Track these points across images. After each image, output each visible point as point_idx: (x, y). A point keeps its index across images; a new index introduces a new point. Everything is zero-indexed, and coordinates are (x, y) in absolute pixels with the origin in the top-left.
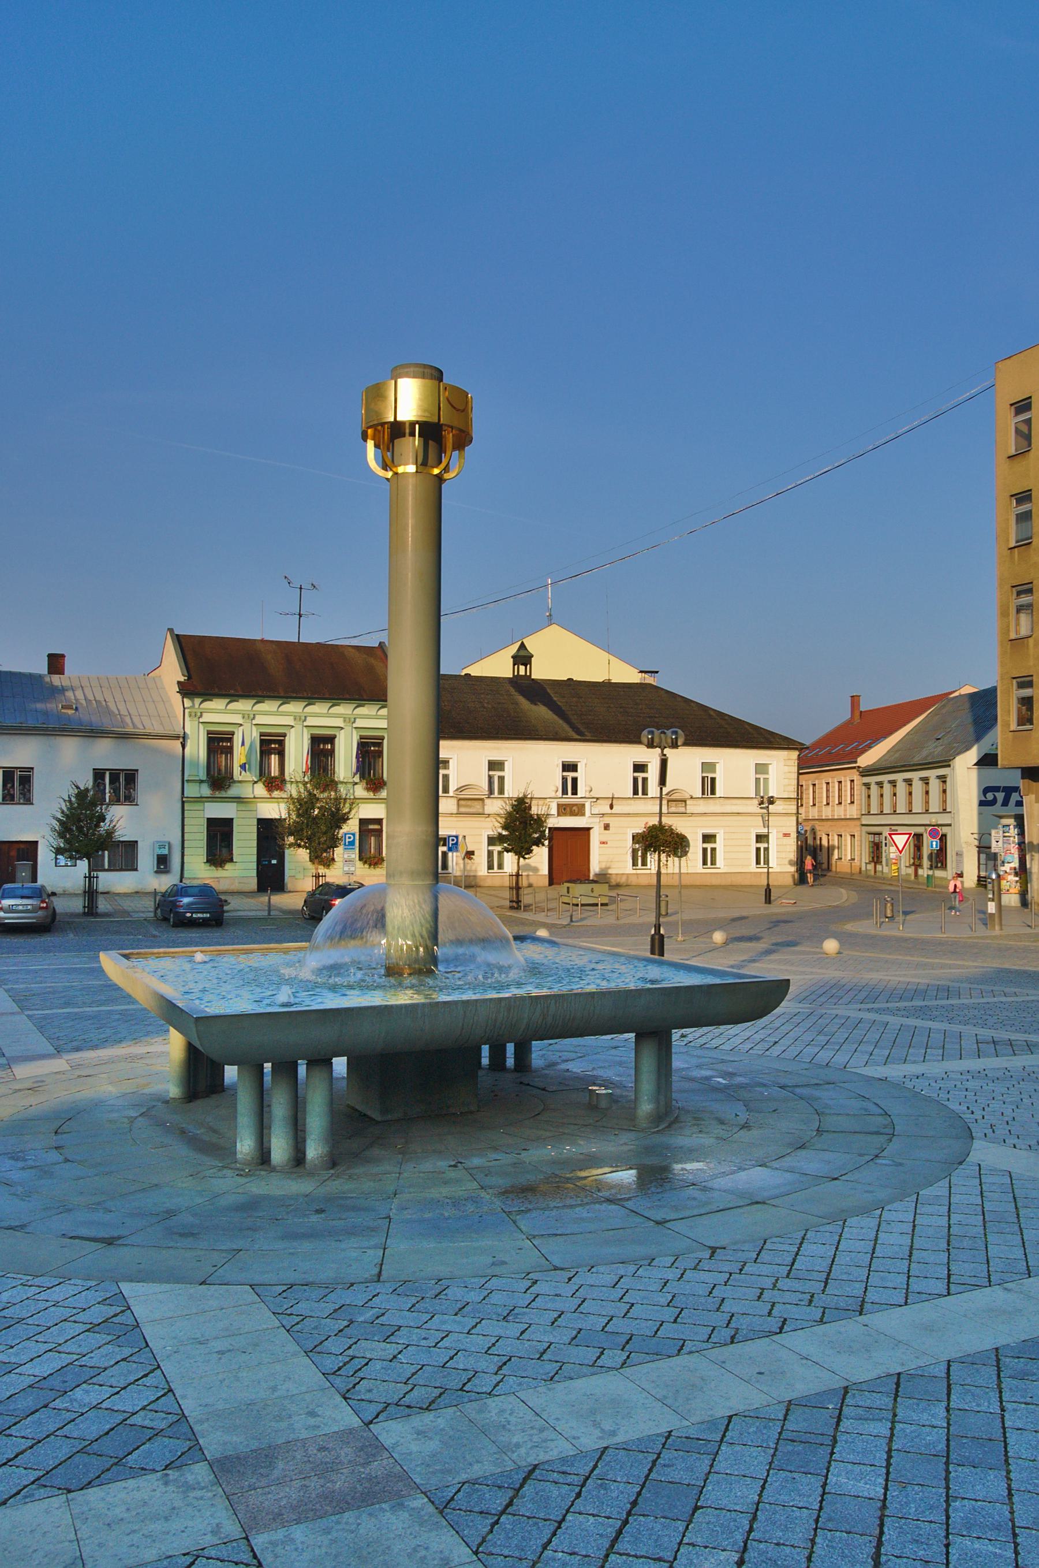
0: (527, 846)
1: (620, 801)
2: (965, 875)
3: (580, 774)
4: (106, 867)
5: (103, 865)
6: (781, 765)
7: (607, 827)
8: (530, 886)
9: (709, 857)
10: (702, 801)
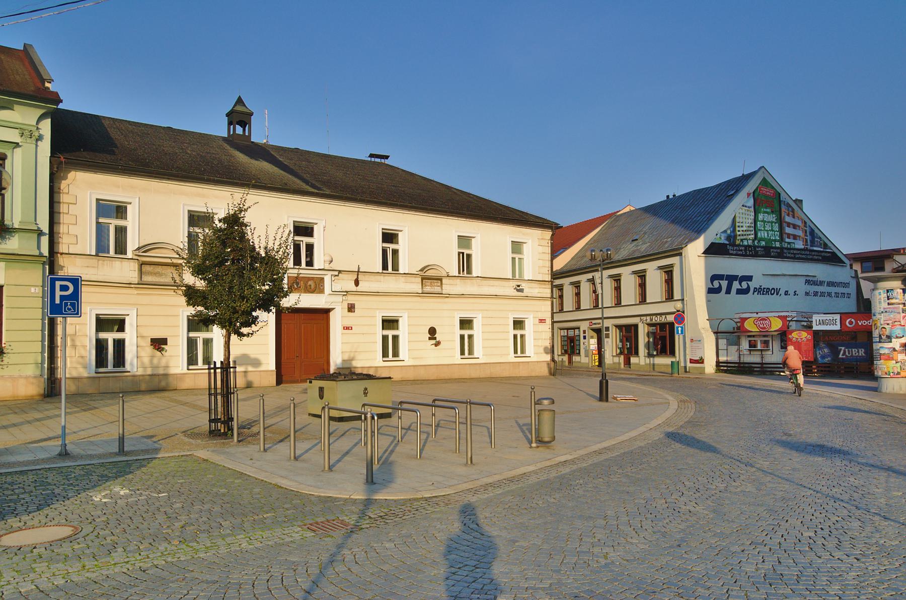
0: (244, 306)
1: (367, 277)
2: (705, 361)
3: (317, 240)
4: (862, 352)
5: (858, 359)
6: (536, 242)
7: (351, 308)
8: (249, 385)
9: (466, 345)
10: (458, 281)
